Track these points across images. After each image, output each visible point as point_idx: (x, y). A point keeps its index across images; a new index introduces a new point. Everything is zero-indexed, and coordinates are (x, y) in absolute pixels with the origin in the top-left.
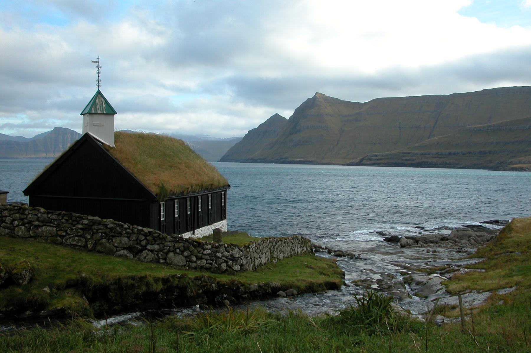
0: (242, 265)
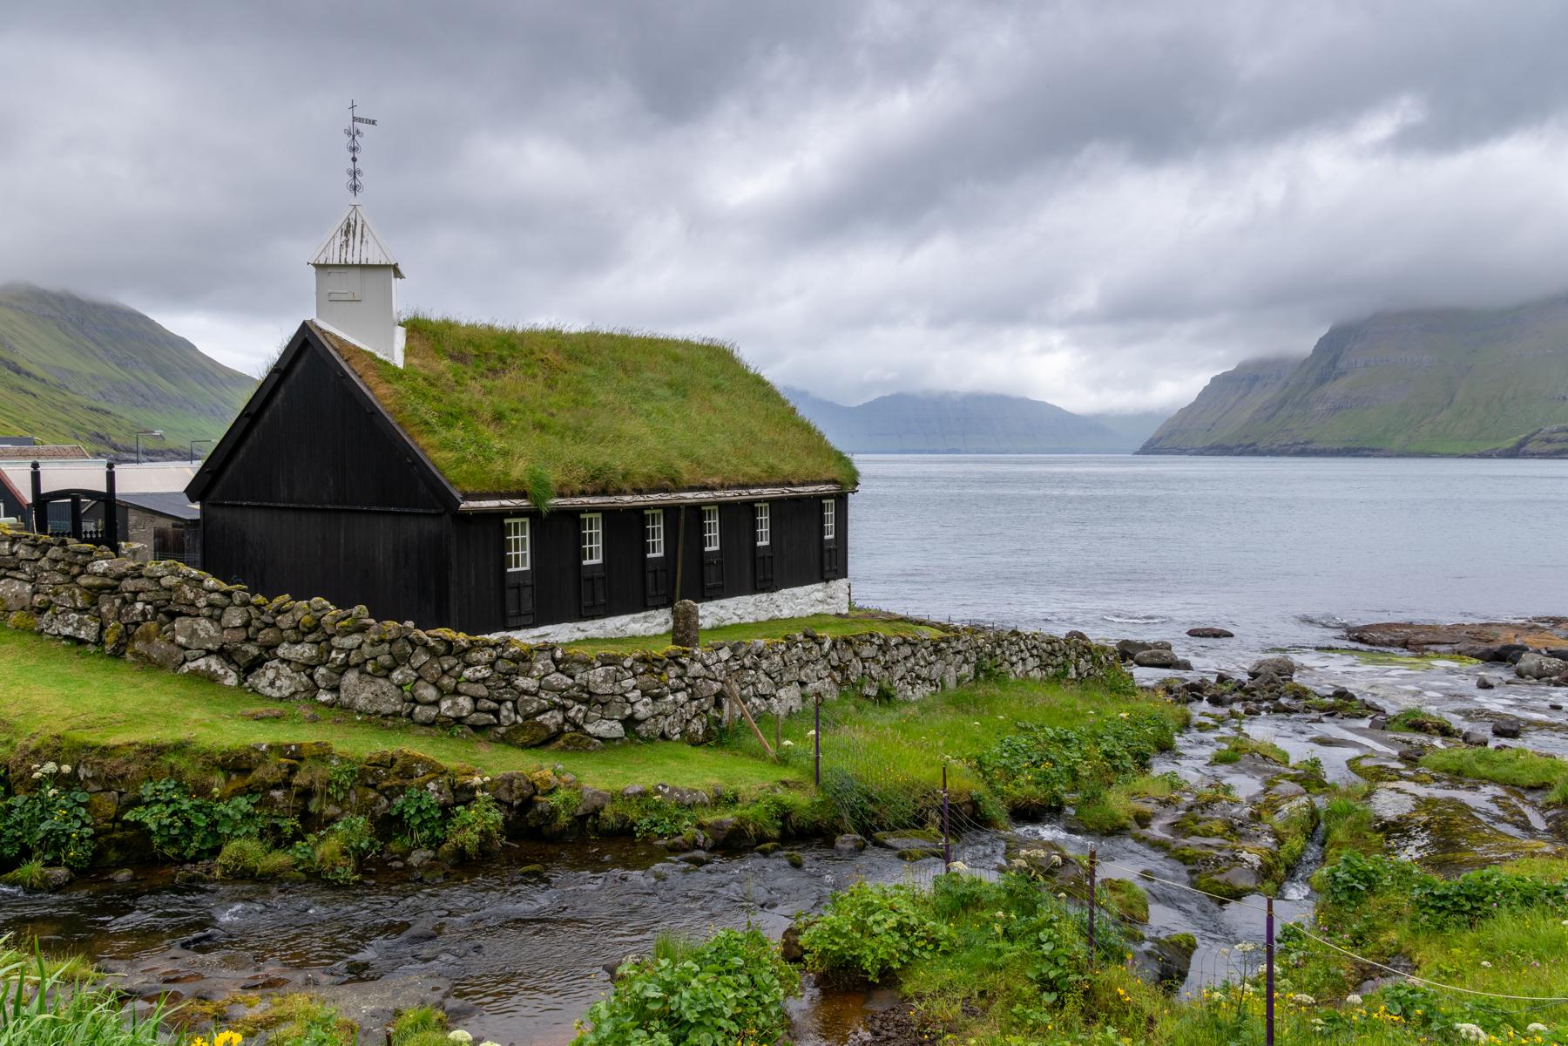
0: (630, 722)
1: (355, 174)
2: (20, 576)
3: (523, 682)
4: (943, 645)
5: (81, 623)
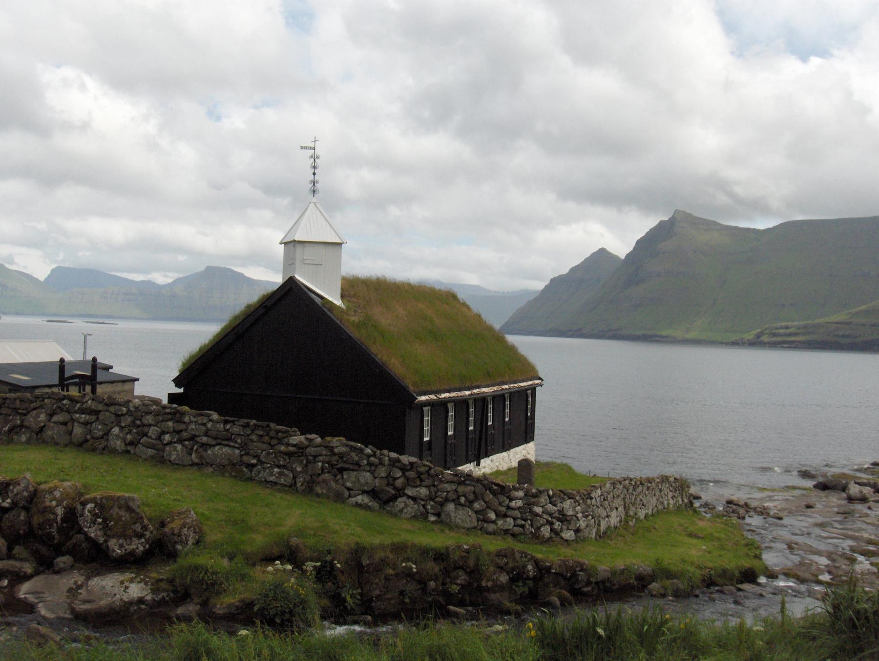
0: (577, 531)
1: (314, 183)
2: (232, 444)
5: (281, 474)
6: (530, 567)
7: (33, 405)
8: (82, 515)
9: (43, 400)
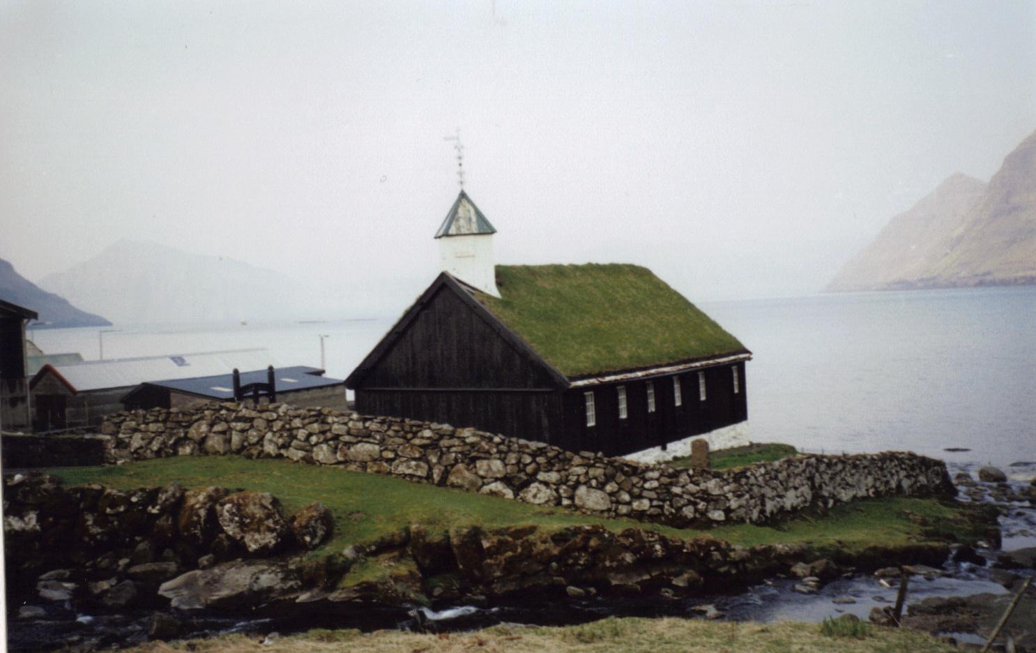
0: (728, 511)
2: (372, 440)
3: (677, 490)
4: (858, 462)
5: (418, 466)
6: (658, 547)
7: (195, 417)
8: (221, 515)
9: (203, 412)
